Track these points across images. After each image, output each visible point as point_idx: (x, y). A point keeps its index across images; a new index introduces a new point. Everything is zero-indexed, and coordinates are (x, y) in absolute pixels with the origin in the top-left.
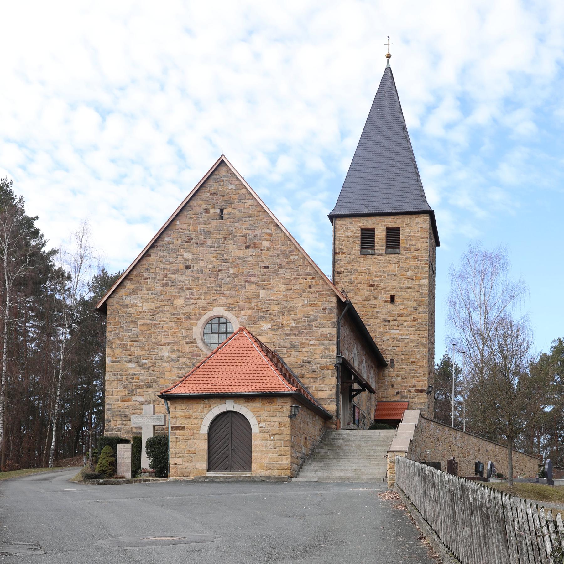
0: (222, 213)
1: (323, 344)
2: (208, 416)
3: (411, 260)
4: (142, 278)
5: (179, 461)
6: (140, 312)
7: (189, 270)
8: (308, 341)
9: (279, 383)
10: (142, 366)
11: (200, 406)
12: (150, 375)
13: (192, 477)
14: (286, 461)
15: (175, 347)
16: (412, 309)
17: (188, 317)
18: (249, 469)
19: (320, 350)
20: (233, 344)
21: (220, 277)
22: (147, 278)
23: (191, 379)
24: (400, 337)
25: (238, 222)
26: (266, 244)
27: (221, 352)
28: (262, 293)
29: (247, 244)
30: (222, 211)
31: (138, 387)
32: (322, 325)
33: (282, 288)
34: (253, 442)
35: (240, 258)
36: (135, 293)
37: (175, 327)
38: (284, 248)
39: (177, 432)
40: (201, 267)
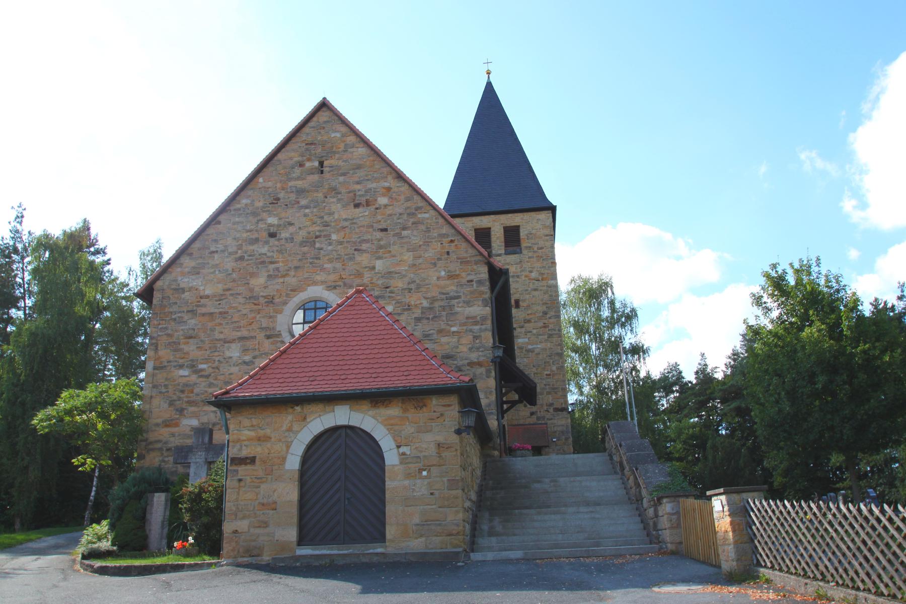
0: (322, 167)
1: (471, 331)
2: (299, 436)
3: (535, 259)
4: (207, 251)
5: (242, 525)
6: (201, 298)
7: (273, 239)
8: (448, 327)
9: (433, 371)
10: (197, 372)
11: (286, 418)
12: (211, 385)
13: (266, 558)
14: (456, 517)
15: (249, 344)
16: (541, 314)
17: (270, 301)
18: (381, 537)
19: (467, 340)
20: (345, 313)
21: (317, 245)
22: (214, 252)
23: (271, 371)
24: (530, 347)
25: (344, 174)
26: (383, 201)
27: (325, 327)
28: (379, 265)
29: (357, 202)
30: (321, 164)
31: (191, 403)
32: (468, 303)
33: (408, 257)
34: (389, 484)
35: (346, 220)
36: (196, 271)
37: (250, 316)
38: (409, 204)
39: (242, 470)
40: (291, 234)
